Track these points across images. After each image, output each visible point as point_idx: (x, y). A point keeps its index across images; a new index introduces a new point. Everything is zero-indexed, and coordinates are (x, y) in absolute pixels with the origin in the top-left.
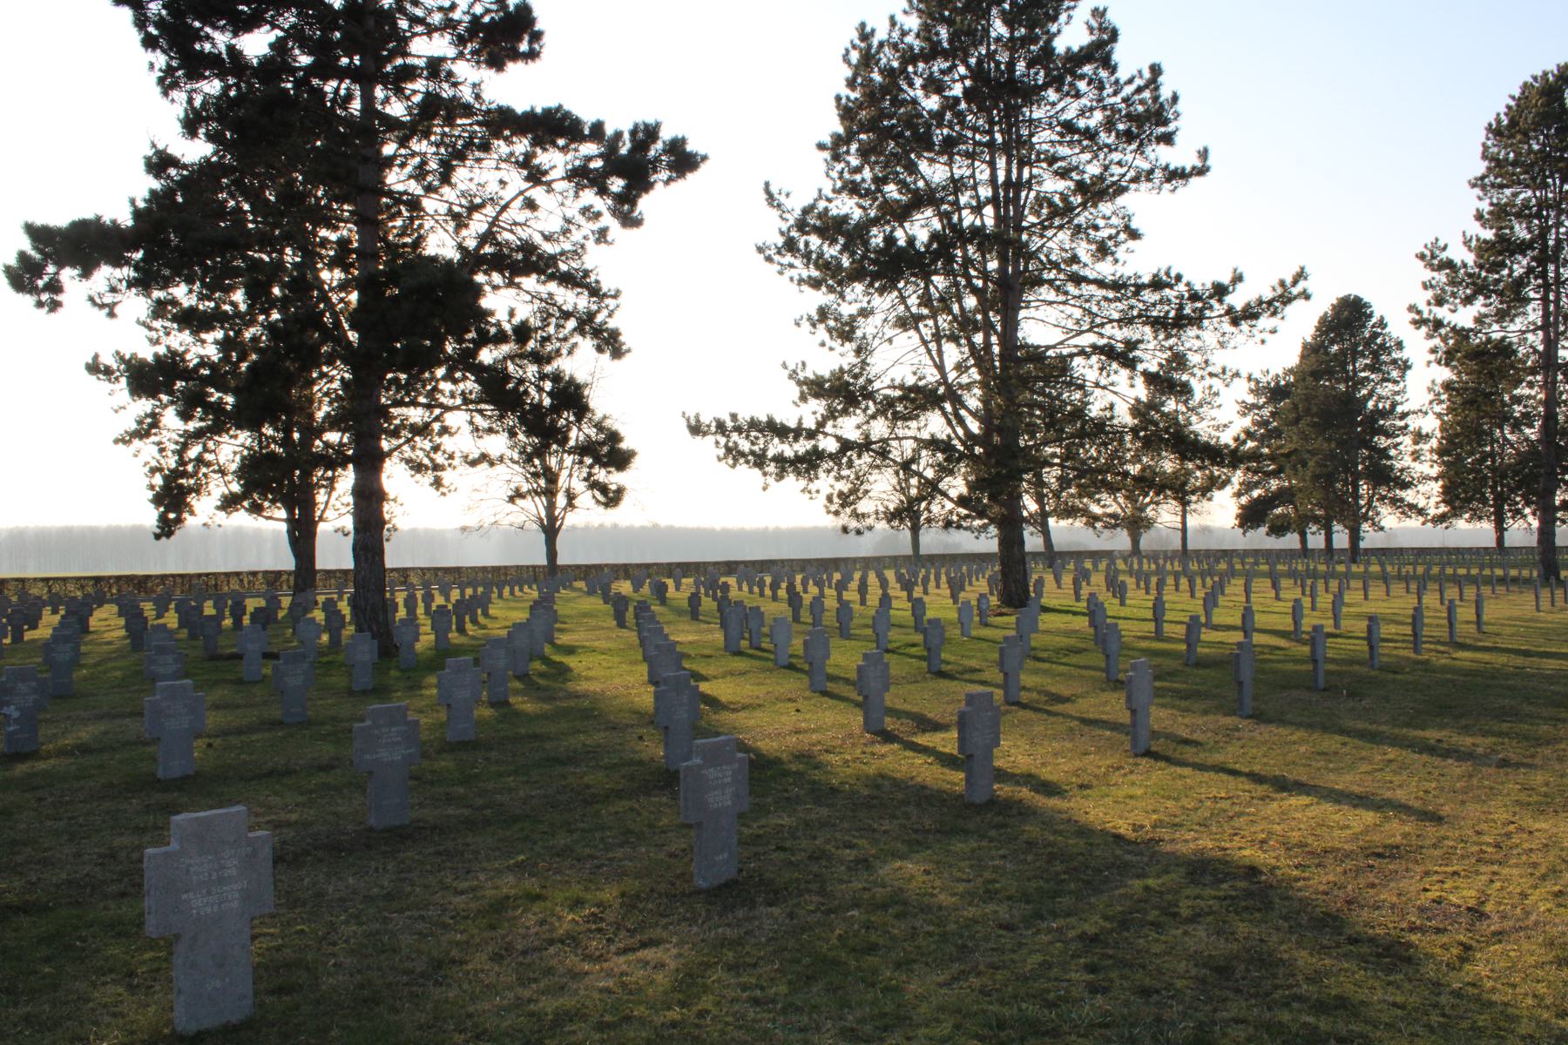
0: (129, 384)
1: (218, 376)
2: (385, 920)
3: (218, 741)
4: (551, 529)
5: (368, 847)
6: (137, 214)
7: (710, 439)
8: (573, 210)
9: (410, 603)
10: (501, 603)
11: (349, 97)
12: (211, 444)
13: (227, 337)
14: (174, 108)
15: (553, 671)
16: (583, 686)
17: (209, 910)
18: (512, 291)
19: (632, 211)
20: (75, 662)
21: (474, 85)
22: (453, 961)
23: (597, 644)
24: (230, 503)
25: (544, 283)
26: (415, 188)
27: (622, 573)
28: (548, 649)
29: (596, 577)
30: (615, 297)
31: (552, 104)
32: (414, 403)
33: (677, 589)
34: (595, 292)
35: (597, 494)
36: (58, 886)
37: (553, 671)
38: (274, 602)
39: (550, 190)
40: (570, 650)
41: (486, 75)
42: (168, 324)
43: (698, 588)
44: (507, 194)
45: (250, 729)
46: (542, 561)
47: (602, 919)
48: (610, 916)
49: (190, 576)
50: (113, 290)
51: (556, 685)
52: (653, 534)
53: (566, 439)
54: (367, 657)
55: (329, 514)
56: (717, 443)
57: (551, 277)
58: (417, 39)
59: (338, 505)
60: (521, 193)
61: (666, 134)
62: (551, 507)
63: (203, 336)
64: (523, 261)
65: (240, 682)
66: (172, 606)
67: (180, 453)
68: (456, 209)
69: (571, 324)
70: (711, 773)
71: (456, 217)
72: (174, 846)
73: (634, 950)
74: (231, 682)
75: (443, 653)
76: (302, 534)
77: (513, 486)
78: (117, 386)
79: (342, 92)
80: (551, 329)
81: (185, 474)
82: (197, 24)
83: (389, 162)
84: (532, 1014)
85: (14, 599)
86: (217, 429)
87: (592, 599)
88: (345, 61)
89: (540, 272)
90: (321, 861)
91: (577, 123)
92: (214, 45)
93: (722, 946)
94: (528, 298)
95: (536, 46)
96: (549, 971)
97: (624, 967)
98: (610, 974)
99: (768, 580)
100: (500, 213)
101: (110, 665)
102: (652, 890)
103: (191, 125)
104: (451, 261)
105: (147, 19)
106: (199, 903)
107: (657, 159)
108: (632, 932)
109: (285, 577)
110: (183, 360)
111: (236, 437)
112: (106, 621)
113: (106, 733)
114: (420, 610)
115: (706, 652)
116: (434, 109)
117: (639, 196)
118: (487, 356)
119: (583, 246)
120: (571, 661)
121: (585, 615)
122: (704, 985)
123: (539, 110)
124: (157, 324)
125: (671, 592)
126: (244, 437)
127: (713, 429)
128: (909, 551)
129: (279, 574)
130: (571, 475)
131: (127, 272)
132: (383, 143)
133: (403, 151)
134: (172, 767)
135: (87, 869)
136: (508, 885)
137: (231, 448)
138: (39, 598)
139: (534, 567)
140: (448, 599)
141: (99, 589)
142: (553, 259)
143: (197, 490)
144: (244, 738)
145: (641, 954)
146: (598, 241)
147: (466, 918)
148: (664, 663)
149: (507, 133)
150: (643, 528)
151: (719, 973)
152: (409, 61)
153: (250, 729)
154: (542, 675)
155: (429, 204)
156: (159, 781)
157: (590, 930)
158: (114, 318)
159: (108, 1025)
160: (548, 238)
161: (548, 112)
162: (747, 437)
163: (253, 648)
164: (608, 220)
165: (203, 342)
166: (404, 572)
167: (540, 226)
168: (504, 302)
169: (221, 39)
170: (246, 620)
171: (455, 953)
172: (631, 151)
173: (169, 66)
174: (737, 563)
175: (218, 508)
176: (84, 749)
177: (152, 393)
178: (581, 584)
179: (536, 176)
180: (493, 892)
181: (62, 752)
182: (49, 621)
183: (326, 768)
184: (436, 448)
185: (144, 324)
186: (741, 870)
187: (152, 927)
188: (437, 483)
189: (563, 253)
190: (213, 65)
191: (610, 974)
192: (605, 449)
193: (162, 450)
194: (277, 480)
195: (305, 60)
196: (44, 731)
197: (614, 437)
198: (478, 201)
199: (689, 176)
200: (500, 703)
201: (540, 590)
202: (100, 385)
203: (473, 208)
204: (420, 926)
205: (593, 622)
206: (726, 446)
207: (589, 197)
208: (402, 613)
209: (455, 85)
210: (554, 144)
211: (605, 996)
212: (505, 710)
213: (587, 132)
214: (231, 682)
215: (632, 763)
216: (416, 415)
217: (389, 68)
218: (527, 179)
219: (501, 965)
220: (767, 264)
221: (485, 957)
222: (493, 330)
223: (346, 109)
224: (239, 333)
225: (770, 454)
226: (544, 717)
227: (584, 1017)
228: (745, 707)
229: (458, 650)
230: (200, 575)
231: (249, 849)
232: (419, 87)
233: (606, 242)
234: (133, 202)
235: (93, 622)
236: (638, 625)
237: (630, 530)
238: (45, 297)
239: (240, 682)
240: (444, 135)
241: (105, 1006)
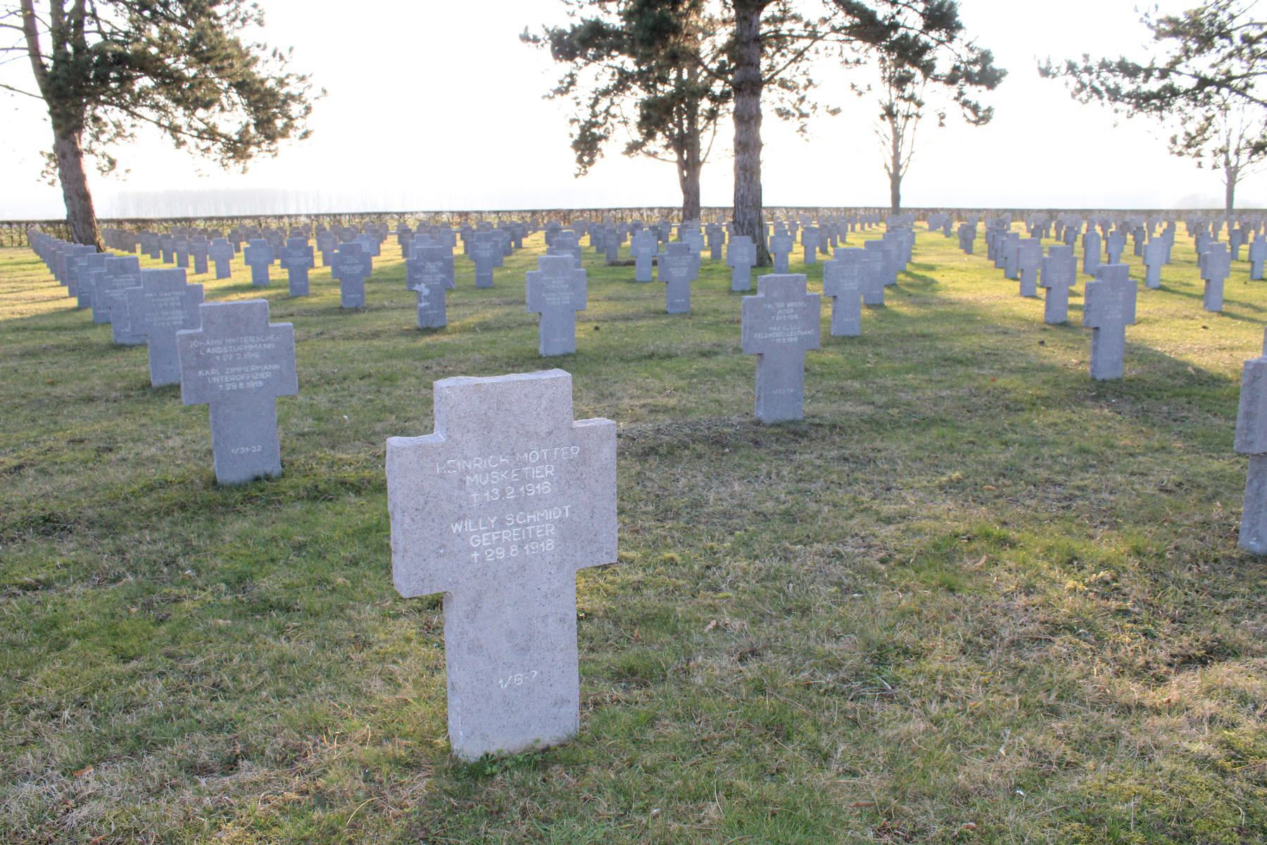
3: (606, 325)
7: (1061, 80)
12: (616, 100)
17: (501, 555)
28: (909, 267)
40: (931, 268)
45: (637, 317)
49: (603, 211)
54: (747, 260)
81: (595, 125)
90: (700, 457)
106: (482, 541)
109: (675, 212)
113: (508, 314)
121: (932, 244)
127: (1063, 70)
128: (1222, 205)
129: (671, 209)
136: (947, 516)
139: (880, 209)
144: (630, 324)
153: (637, 317)
154: (909, 285)
156: (540, 357)
171: (904, 636)
176: (485, 327)
177: (570, 56)
196: (450, 313)
200: (877, 306)
204: (837, 570)
205: (941, 250)
212: (880, 311)
226: (925, 319)
231: (575, 451)
235: (525, 241)
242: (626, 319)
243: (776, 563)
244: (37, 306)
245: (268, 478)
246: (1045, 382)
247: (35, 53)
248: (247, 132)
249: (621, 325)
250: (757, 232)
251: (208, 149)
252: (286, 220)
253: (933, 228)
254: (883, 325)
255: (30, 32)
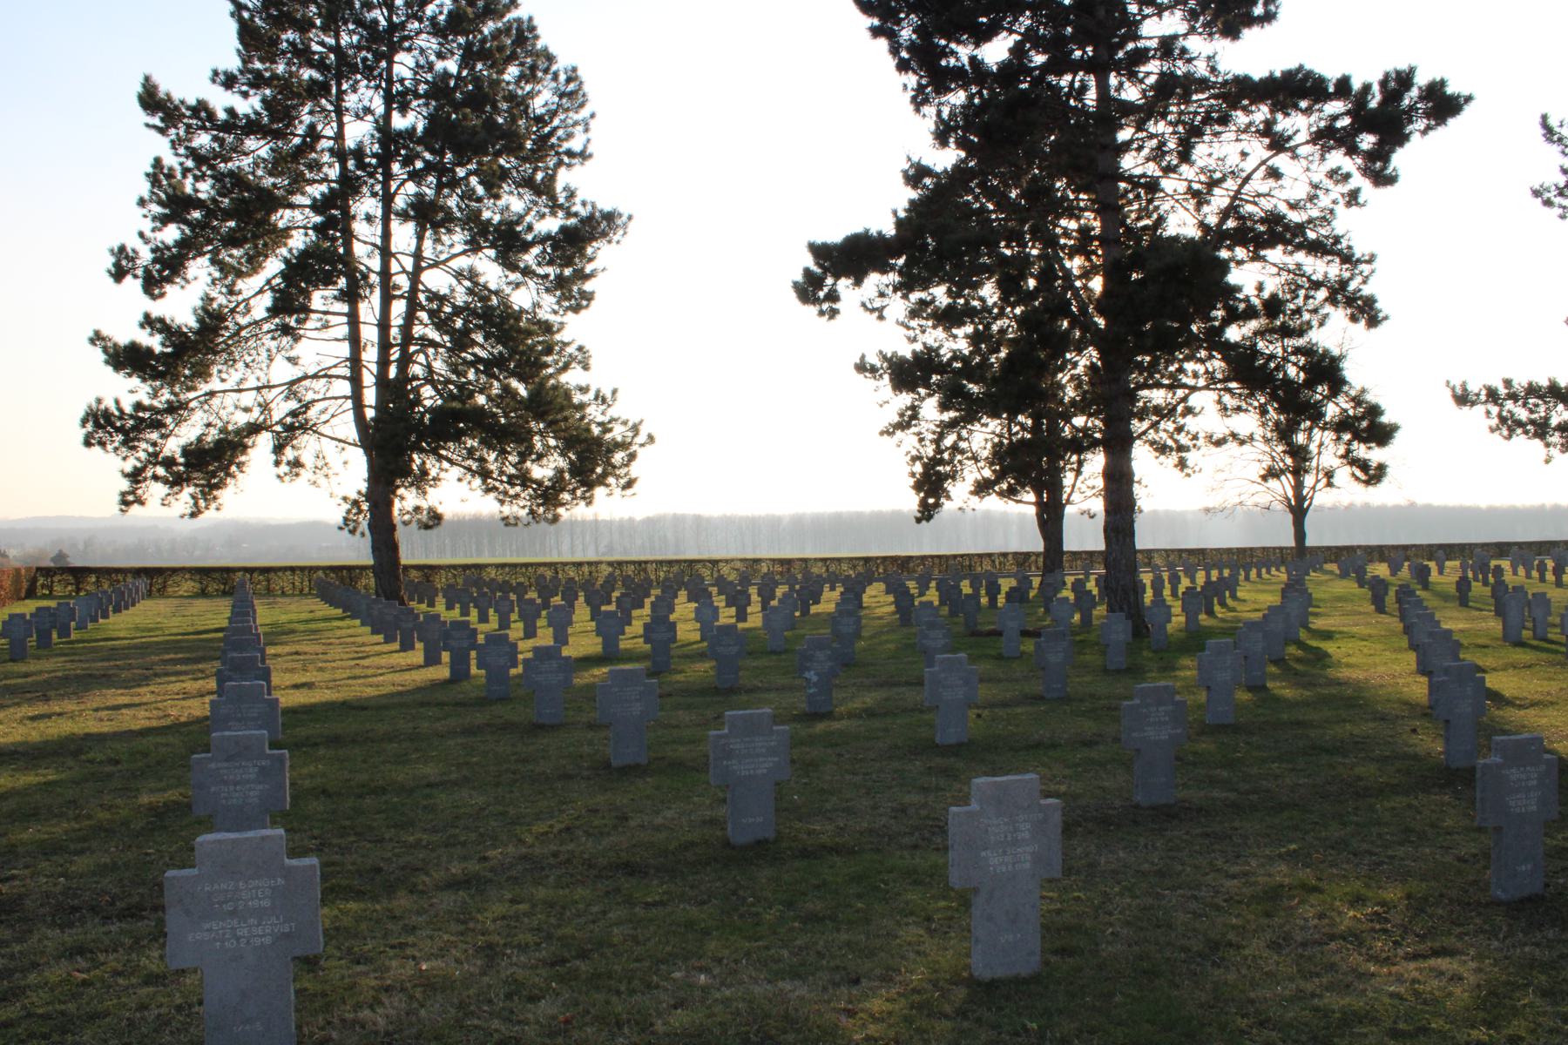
0: (891, 380)
1: (970, 370)
2: (1158, 896)
4: (1298, 510)
5: (1135, 822)
6: (900, 224)
7: (1480, 409)
8: (1319, 175)
9: (1157, 586)
10: (1248, 586)
11: (1084, 88)
12: (964, 433)
13: (976, 330)
14: (926, 123)
15: (1310, 656)
16: (1344, 673)
18: (1257, 265)
19: (1384, 168)
20: (857, 635)
21: (1209, 58)
22: (1230, 945)
23: (1355, 629)
24: (982, 488)
25: (1291, 253)
26: (1152, 169)
27: (1376, 555)
28: (1303, 634)
29: (1350, 559)
30: (1369, 262)
31: (1292, 65)
32: (1158, 385)
33: (1441, 572)
34: (1347, 258)
35: (1358, 473)
36: (861, 833)
37: (1310, 656)
38: (1025, 582)
39: (1295, 157)
40: (1327, 635)
41: (1221, 45)
42: (923, 322)
43: (1464, 571)
44: (1248, 166)
46: (1289, 542)
47: (1387, 920)
48: (1396, 917)
50: (882, 295)
51: (1315, 671)
52: (1411, 513)
53: (1322, 415)
55: (1074, 497)
56: (1488, 413)
57: (1299, 247)
58: (1147, 21)
59: (1084, 488)
60: (1263, 163)
61: (1421, 80)
62: (1298, 486)
63: (955, 331)
64: (1275, 231)
65: (1000, 657)
66: (933, 584)
67: (937, 442)
68: (1196, 186)
69: (1322, 294)
70: (1514, 774)
71: (1195, 194)
72: (974, 806)
73: (1425, 957)
74: (993, 657)
75: (1194, 640)
76: (1051, 517)
77: (1265, 465)
78: (881, 383)
79: (1077, 85)
80: (1300, 302)
81: (942, 462)
82: (943, 42)
83: (1126, 147)
84: (1316, 1009)
85: (799, 577)
86: (970, 418)
87: (1345, 583)
88: (1078, 54)
89: (1286, 243)
90: (1091, 832)
91: (1321, 81)
92: (958, 59)
93: (1532, 967)
94: (1275, 270)
95: (1272, 8)
96: (1332, 967)
97: (1416, 974)
98: (1400, 979)
99: (1550, 564)
100: (1241, 186)
101: (884, 638)
102: (1442, 895)
103: (941, 137)
104: (1193, 239)
105: (900, 45)
107: (1412, 108)
108: (1422, 938)
110: (938, 355)
111: (986, 425)
112: (877, 598)
113: (887, 699)
114: (1167, 592)
115: (1480, 641)
116: (1171, 88)
117: (1393, 151)
118: (1234, 334)
119: (1332, 212)
120: (1329, 647)
121: (1339, 599)
122: (1514, 1007)
123: (1278, 74)
124: (914, 323)
125: (1434, 576)
126: (994, 425)
127: (1483, 398)
129: (1027, 555)
130: (1326, 449)
131: (893, 277)
132: (1121, 127)
133: (1140, 135)
134: (949, 735)
135: (884, 820)
136: (1281, 873)
137: (984, 435)
138: (820, 576)
139: (1281, 549)
140: (1193, 580)
141: (869, 569)
142: (1300, 228)
143: (953, 476)
145: (1432, 962)
146: (1348, 205)
147: (1239, 902)
148: (1432, 649)
149: (1245, 102)
150: (1397, 508)
151: (1529, 998)
152: (1141, 44)
154: (1299, 660)
155: (1168, 184)
157: (1373, 930)
158: (877, 317)
159: (915, 961)
160: (1293, 206)
161: (1289, 75)
162: (1524, 405)
163: (1012, 626)
164: (1358, 180)
165: (955, 337)
166: (1149, 553)
167: (1285, 195)
168: (1250, 277)
169: (964, 52)
170: (1001, 600)
171: (1231, 936)
172: (1381, 104)
173: (919, 85)
174: (1509, 545)
175: (972, 493)
176: (870, 713)
177: (912, 388)
178: (1333, 567)
179: (1279, 143)
180: (1267, 879)
181: (851, 715)
182: (829, 601)
183: (1089, 744)
184: (1180, 429)
185: (902, 324)
186: (1547, 885)
187: (955, 878)
188: (1182, 464)
189: (1310, 221)
190: (959, 77)
191: (1400, 979)
192: (1364, 424)
193: (921, 440)
194: (1030, 467)
195: (1039, 59)
196: (837, 695)
197: (1374, 411)
198: (1218, 175)
199: (1451, 122)
200: (1258, 688)
201: (1288, 572)
202: (865, 382)
203: (1213, 184)
204: (1193, 905)
205: (1349, 607)
206: (1500, 416)
207: (1337, 158)
208: (1148, 596)
209: (1189, 61)
210: (1296, 107)
211: (1397, 1002)
213: (1331, 90)
214: (993, 657)
215: (1406, 756)
216: (1158, 397)
217: (1121, 54)
218: (1270, 147)
219: (1279, 953)
220: (1546, 209)
221: (1262, 944)
222: (1242, 306)
223: (1081, 100)
224: (988, 327)
225: (1554, 422)
226: (1306, 703)
227: (1374, 1021)
228: (1533, 704)
229: (1209, 632)
230: (955, 556)
231: (1041, 816)
232: (1153, 67)
233: (1357, 204)
234: (895, 213)
236: (1401, 610)
237: (1382, 509)
238: (825, 306)
239: (1000, 657)
240: (1181, 113)
241: (909, 944)
242: (1005, 705)
243: (1151, 901)
244: (407, 676)
245: (767, 841)
246: (1399, 771)
247: (359, 407)
248: (563, 478)
249: (1000, 712)
250: (1132, 598)
251: (517, 496)
252: (586, 569)
253: (1344, 575)
254: (1260, 711)
255: (356, 380)
